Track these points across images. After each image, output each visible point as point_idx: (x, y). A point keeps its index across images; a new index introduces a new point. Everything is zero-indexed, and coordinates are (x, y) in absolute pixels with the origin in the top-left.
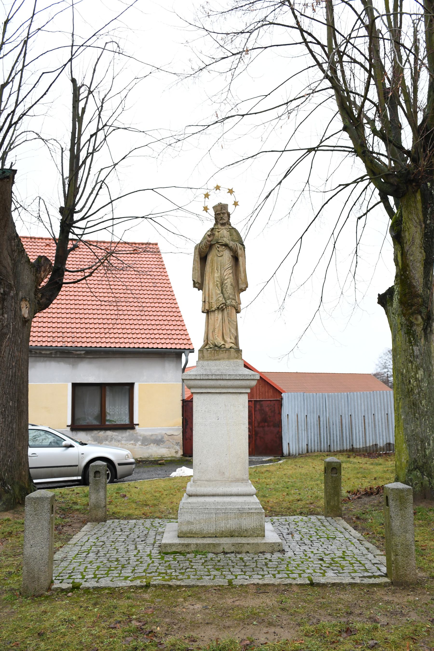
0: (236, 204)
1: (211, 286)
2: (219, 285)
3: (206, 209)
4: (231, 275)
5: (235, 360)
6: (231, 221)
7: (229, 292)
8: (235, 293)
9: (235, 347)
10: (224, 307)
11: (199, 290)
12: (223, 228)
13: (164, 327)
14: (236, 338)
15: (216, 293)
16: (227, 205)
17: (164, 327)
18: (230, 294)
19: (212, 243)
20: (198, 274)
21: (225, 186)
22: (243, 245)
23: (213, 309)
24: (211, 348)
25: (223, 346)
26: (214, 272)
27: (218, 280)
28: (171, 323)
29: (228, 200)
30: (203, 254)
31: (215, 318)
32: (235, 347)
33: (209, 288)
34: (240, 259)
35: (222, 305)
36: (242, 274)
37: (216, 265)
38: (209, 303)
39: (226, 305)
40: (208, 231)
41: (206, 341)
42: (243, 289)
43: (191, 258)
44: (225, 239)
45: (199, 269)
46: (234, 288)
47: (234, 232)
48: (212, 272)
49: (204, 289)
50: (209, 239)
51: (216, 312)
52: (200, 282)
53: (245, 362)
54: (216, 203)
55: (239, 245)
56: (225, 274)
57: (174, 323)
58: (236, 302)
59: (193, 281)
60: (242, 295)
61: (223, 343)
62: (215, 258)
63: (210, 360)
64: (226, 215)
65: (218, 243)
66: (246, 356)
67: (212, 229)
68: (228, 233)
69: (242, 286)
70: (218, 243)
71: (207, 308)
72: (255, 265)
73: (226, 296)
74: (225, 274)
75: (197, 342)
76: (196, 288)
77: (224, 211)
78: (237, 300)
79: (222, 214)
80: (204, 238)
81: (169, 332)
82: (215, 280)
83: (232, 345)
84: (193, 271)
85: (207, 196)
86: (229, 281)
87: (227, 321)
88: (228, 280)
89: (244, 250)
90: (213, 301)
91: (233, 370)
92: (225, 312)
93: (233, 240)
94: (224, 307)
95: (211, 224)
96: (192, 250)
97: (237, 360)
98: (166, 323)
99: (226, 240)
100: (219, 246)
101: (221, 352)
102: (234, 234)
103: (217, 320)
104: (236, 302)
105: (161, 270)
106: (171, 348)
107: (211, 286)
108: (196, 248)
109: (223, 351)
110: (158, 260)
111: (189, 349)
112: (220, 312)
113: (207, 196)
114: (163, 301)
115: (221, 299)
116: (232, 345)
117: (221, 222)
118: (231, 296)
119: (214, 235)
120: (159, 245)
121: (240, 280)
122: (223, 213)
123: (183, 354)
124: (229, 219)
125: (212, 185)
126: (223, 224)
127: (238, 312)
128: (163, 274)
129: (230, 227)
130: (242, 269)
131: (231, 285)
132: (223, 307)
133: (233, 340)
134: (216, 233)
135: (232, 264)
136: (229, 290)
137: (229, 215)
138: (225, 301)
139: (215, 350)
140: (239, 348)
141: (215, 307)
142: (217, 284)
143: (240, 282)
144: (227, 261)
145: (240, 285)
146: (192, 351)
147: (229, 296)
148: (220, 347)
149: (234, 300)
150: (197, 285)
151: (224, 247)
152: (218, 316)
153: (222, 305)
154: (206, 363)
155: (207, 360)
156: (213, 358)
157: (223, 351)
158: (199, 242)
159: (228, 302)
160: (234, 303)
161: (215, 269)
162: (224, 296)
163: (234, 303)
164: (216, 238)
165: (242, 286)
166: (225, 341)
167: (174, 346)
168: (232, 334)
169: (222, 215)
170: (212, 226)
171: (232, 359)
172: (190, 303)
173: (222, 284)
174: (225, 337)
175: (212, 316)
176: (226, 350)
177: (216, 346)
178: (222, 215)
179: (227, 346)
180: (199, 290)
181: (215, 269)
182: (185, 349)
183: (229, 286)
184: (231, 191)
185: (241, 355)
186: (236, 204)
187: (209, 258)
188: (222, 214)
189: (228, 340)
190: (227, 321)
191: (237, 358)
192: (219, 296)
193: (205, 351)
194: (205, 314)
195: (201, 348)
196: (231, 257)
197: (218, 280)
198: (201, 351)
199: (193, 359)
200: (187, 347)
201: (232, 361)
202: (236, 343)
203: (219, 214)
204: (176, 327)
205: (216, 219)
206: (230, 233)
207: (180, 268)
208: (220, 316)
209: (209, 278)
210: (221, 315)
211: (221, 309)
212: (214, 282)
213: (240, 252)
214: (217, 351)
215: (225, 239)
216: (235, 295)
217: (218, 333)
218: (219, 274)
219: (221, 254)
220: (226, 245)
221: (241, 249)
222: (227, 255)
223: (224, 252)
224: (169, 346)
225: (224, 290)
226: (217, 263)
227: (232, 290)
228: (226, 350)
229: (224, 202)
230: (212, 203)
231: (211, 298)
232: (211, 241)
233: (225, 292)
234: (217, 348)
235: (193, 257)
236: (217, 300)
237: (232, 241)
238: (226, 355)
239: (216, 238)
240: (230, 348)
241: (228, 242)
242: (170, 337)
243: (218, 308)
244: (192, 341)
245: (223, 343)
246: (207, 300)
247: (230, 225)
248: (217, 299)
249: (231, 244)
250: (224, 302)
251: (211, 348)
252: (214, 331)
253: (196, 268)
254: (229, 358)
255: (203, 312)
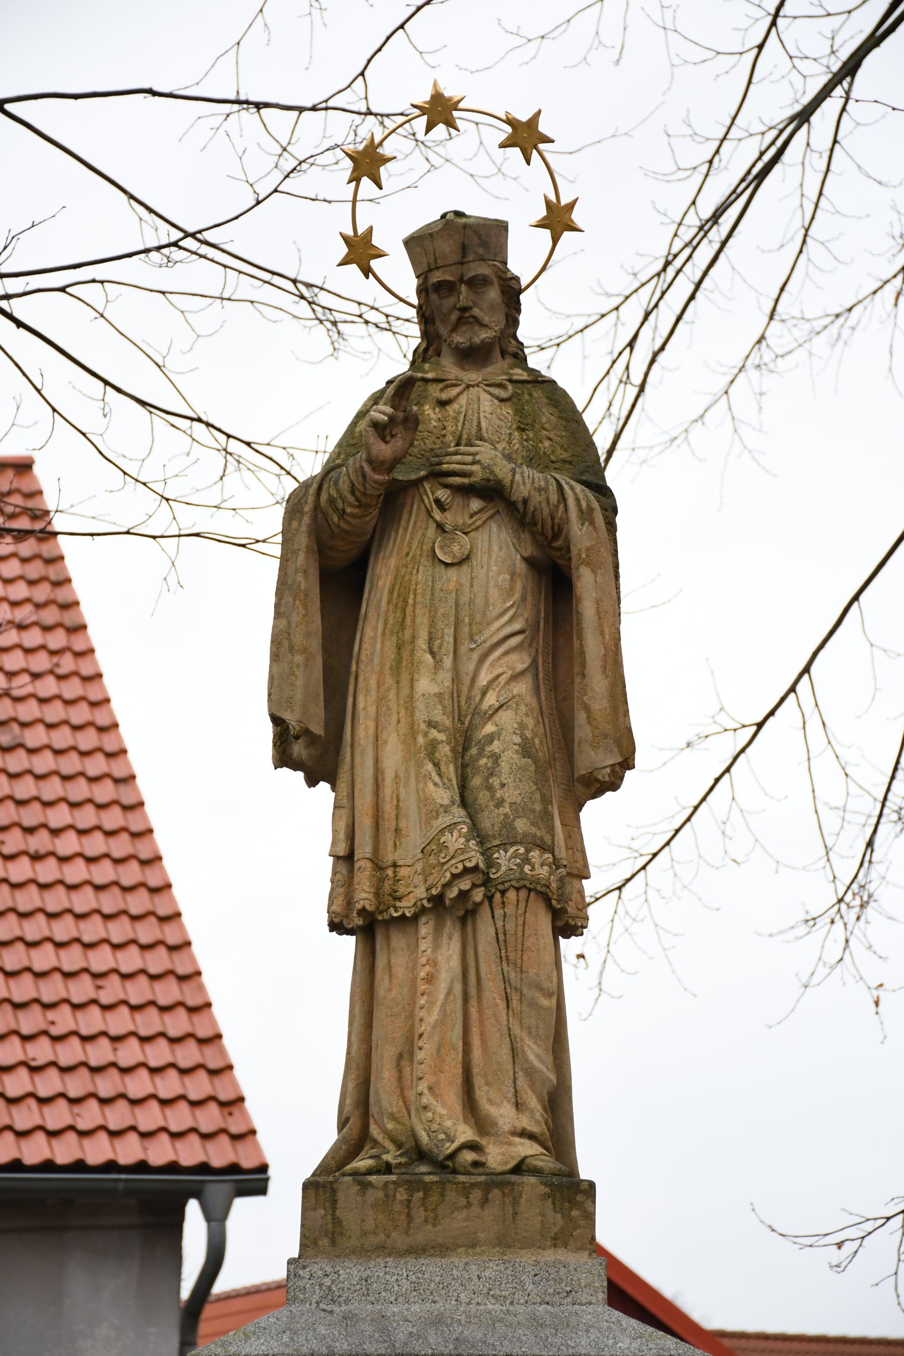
0: (558, 220)
1: (393, 756)
2: (445, 750)
3: (361, 251)
4: (522, 688)
5: (549, 1256)
6: (528, 331)
7: (511, 794)
8: (546, 801)
9: (547, 1163)
10: (478, 895)
11: (312, 782)
12: (473, 376)
13: (64, 1020)
14: (558, 1102)
15: (424, 801)
16: (502, 227)
17: (64, 1020)
18: (519, 810)
19: (401, 475)
20: (310, 676)
21: (493, 92)
22: (603, 492)
23: (406, 907)
24: (388, 1169)
25: (469, 1156)
26: (414, 668)
27: (438, 715)
28: (112, 991)
29: (507, 194)
30: (341, 543)
31: (413, 967)
32: (547, 1163)
33: (378, 772)
34: (586, 582)
35: (465, 884)
36: (598, 683)
37: (423, 620)
38: (378, 866)
39: (487, 882)
40: (376, 398)
41: (354, 1123)
42: (604, 775)
43: (263, 572)
44: (485, 452)
45: (315, 644)
46: (541, 779)
47: (545, 406)
48: (402, 664)
49: (343, 784)
50: (384, 450)
51: (425, 928)
52: (318, 729)
53: (613, 1264)
54: (425, 213)
55: (576, 492)
56: (484, 678)
57: (138, 991)
58: (556, 864)
59: (276, 720)
60: (595, 814)
61: (465, 1133)
62: (422, 575)
63: (382, 1250)
64: (493, 294)
65: (437, 475)
66: (613, 1229)
67: (402, 390)
68: (507, 411)
69: (595, 758)
70: (437, 475)
71: (364, 897)
72: (680, 628)
73: (490, 820)
74: (484, 678)
75: (294, 1116)
76: (295, 766)
77: (483, 270)
78: (562, 852)
79: (464, 283)
80: (350, 442)
81: (100, 1053)
82: (421, 715)
83: (527, 1149)
84: (275, 657)
85: (367, 163)
86: (510, 725)
87: (493, 991)
88: (507, 718)
89: (612, 527)
90: (407, 852)
91: (537, 1323)
92: (485, 928)
93: (534, 459)
94: (478, 895)
95: (392, 354)
96: (272, 521)
97: (561, 1255)
98: (82, 989)
99: (490, 458)
100: (443, 494)
101: (451, 1195)
102: (547, 416)
103: (430, 979)
104: (556, 864)
105: (57, 640)
106: (111, 1166)
107: (393, 756)
108: (294, 507)
109: (466, 1190)
110: (34, 570)
111: (234, 1168)
112: (450, 927)
113: (367, 163)
114: (68, 844)
115: (454, 841)
116: (527, 1149)
117: (459, 339)
118: (522, 825)
119: (411, 422)
120: (44, 474)
121: (581, 717)
122: (477, 283)
123: (193, 1208)
124: (513, 322)
125: (401, 86)
126: (473, 356)
127: (568, 923)
128: (67, 664)
129: (519, 374)
130: (592, 646)
131: (526, 750)
132: (469, 897)
133: (534, 1119)
134: (430, 412)
135: (527, 613)
136: (510, 783)
137: (511, 292)
138: (486, 853)
139: (414, 1185)
140: (572, 1171)
141: (415, 893)
142: (433, 746)
143: (583, 731)
144: (494, 593)
145: (583, 744)
146: (253, 1181)
147: (508, 824)
148: (446, 1165)
149: (544, 848)
150: (298, 749)
151: (476, 504)
152: (439, 954)
153: (465, 884)
154: (351, 1272)
155: (363, 1253)
156: (398, 1239)
157: (466, 1190)
158: (317, 470)
159: (505, 860)
160: (544, 872)
161: (422, 642)
162: (474, 825)
163: (539, 867)
164: (424, 442)
165: (595, 758)
166: (482, 1124)
167: (129, 1151)
168: (530, 1073)
169: (464, 295)
170: (400, 366)
171: (529, 1244)
172: (251, 878)
173: (465, 742)
174: (482, 1093)
175: (396, 954)
176: (487, 1187)
177: (420, 1154)
178: (464, 295)
179: (496, 1156)
180: (312, 782)
181: (422, 642)
182: (204, 1168)
183: (510, 758)
184: (525, 136)
185: (590, 1217)
186: (558, 220)
187: (383, 575)
188: (464, 283)
189: (503, 1114)
190: (493, 991)
191: (559, 1240)
192: (444, 820)
193: (347, 1189)
194: (350, 941)
195: (323, 1169)
196: (521, 567)
197: (438, 715)
198: (319, 1190)
199: (262, 1240)
200: (220, 1154)
201: (526, 1258)
202: (558, 1135)
203: (446, 288)
204: (149, 1022)
205: (426, 317)
206: (519, 412)
207: (183, 651)
208: (449, 955)
209: (381, 701)
210: (457, 936)
211: (454, 908)
212: (413, 732)
213: (580, 535)
214: (426, 1188)
215: (485, 452)
216: (546, 816)
217: (438, 1069)
218: (445, 677)
219: (460, 545)
220: (492, 492)
221: (586, 516)
222: (495, 556)
223: (481, 538)
224: (97, 1151)
225: (476, 781)
226: (432, 610)
227: (529, 787)
228: (487, 1187)
229: (479, 208)
230: (400, 211)
231: (388, 838)
232: (397, 461)
233: (483, 797)
234: (430, 1171)
235: (273, 567)
236: (433, 847)
237: (530, 461)
238: (486, 1219)
239: (424, 442)
240: (519, 1169)
241: (503, 470)
242: (105, 1086)
243: (438, 901)
244: (257, 1110)
245: (465, 1133)
246: (364, 849)
247: (520, 358)
248: (429, 839)
249: (526, 482)
250: (475, 858)
251: (388, 1169)
252: (406, 1055)
253: (298, 639)
254: (505, 1242)
255: (336, 926)
